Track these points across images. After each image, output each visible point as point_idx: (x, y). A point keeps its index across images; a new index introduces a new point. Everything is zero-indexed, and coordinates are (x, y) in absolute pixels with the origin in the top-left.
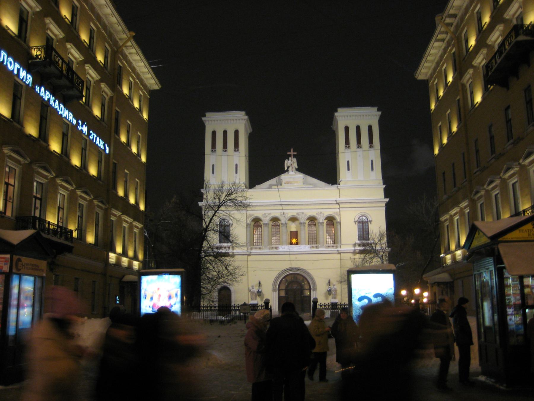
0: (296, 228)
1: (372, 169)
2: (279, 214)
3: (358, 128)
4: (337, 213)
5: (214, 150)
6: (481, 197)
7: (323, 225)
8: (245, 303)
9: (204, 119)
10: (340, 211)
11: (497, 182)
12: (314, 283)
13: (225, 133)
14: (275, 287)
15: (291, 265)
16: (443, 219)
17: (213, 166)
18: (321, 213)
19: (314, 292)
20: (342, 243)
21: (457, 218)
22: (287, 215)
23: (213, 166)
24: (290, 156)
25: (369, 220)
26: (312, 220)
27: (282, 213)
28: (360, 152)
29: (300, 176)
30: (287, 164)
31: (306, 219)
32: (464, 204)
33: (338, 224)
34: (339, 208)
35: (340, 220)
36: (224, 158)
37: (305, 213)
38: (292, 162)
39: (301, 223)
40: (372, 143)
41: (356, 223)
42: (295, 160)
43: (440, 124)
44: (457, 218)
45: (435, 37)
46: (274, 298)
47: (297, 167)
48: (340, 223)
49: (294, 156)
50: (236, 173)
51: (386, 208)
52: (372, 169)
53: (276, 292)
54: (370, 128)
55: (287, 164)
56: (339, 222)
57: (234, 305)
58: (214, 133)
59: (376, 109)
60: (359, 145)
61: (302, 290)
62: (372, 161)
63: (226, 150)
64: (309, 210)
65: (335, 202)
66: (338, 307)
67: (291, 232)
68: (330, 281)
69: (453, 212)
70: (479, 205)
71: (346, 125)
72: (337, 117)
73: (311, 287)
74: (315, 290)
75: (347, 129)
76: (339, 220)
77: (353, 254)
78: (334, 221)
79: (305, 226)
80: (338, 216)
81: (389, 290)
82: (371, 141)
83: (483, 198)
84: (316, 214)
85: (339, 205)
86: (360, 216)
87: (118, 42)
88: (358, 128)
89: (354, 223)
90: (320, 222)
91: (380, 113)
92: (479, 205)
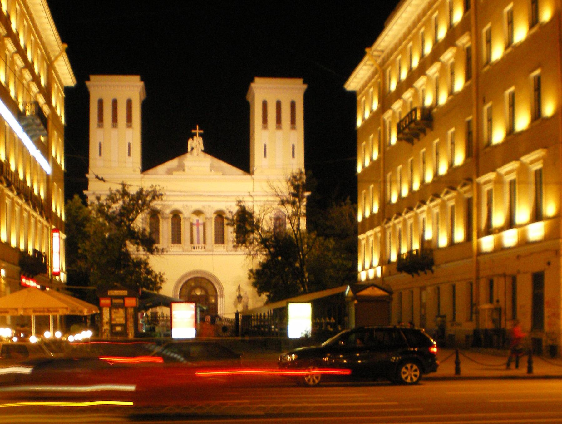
3: (279, 104)
7: (212, 221)
9: (88, 83)
12: (175, 291)
13: (115, 103)
15: (57, 268)
17: (100, 145)
19: (222, 298)
23: (100, 145)
24: (195, 134)
26: (220, 215)
28: (279, 133)
29: (208, 160)
30: (191, 144)
32: (377, 229)
34: (253, 202)
36: (114, 133)
38: (197, 144)
42: (200, 140)
49: (200, 135)
50: (129, 155)
54: (293, 105)
55: (191, 144)
58: (101, 102)
59: (300, 81)
66: (160, 319)
68: (240, 288)
69: (369, 233)
71: (278, 99)
72: (253, 89)
73: (218, 293)
74: (222, 296)
75: (265, 104)
82: (293, 121)
85: (253, 198)
87: (440, 2)
88: (279, 104)
91: (305, 86)
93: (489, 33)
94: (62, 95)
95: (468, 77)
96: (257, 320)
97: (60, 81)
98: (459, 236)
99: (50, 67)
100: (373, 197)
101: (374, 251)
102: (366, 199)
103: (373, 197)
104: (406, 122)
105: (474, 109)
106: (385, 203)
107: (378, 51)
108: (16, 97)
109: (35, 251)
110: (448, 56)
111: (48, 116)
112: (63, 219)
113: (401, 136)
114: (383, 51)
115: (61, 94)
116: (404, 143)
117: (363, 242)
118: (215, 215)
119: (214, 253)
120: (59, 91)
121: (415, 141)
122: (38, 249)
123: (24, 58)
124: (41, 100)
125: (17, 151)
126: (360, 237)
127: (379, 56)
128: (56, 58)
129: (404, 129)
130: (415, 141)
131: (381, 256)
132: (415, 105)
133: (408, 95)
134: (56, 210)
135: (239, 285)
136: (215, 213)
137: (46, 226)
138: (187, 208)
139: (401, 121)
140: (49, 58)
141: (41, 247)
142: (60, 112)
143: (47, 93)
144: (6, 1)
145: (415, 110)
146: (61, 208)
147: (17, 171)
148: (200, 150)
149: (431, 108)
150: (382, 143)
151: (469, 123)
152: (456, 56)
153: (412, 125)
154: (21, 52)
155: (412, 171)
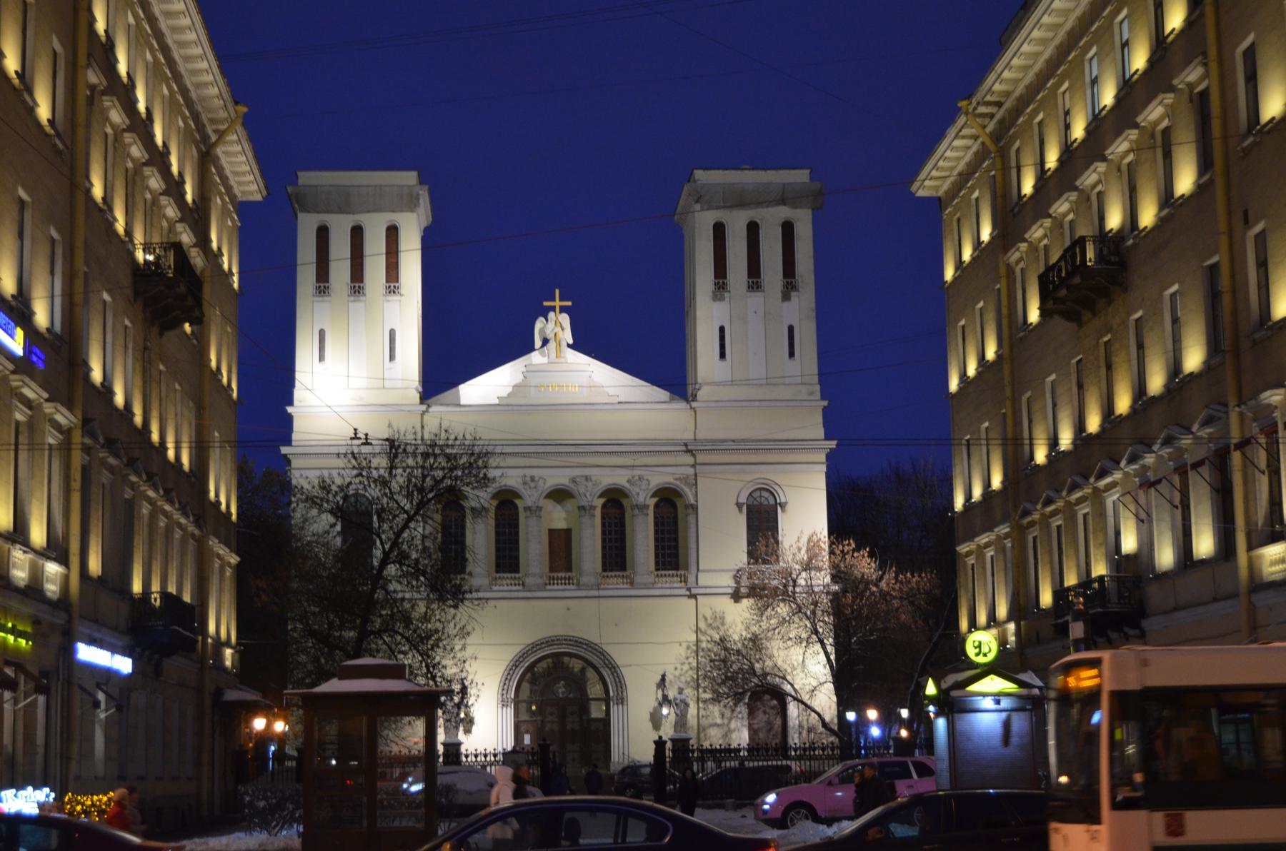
0: (566, 519)
1: (792, 354)
2: (520, 480)
4: (687, 477)
5: (325, 287)
6: (1032, 524)
7: (647, 515)
8: (655, 742)
10: (696, 475)
11: (1058, 504)
14: (505, 692)
16: (963, 549)
18: (640, 478)
19: (620, 706)
20: (701, 568)
21: (990, 553)
22: (541, 483)
25: (778, 501)
26: (615, 501)
27: (528, 479)
28: (756, 299)
31: (598, 494)
32: (1004, 529)
33: (691, 511)
34: (694, 466)
35: (697, 501)
37: (593, 478)
39: (582, 508)
40: (793, 276)
41: (740, 511)
42: (565, 319)
43: (962, 322)
44: (990, 553)
45: (956, 131)
46: (57, 692)
47: (571, 342)
48: (695, 508)
51: (828, 467)
52: (792, 354)
53: (509, 709)
55: (542, 331)
56: (692, 505)
57: (739, 745)
60: (755, 281)
61: (583, 703)
62: (791, 329)
63: (359, 287)
64: (607, 471)
65: (684, 448)
67: (551, 532)
69: (983, 539)
70: (1030, 538)
73: (611, 694)
76: (692, 501)
77: (731, 598)
78: (679, 503)
79: (593, 516)
80: (691, 490)
81: (711, 609)
83: (1037, 527)
84: (629, 481)
85: (694, 455)
86: (752, 489)
89: (736, 509)
90: (637, 505)
92: (1030, 538)
93: (1250, 54)
94: (233, 221)
95: (1205, 165)
96: (414, 454)
97: (229, 189)
98: (1204, 545)
99: (206, 159)
100: (1054, 405)
101: (1040, 568)
102: (972, 457)
103: (1054, 405)
104: (1060, 270)
105: (1224, 240)
106: (1018, 465)
107: (988, 104)
108: (129, 232)
109: (165, 595)
110: (1154, 113)
111: (203, 271)
112: (234, 517)
113: (1050, 304)
114: (999, 104)
115: (233, 220)
116: (1058, 323)
117: (971, 561)
118: (495, 503)
119: (602, 593)
120: (224, 213)
121: (1086, 315)
122: (172, 589)
123: (148, 139)
124: (186, 238)
125: (130, 360)
126: (963, 549)
127: (992, 116)
128: (221, 134)
129: (1056, 288)
130: (1086, 315)
131: (1014, 594)
132: (1082, 231)
133: (1062, 207)
134: (217, 495)
135: (662, 673)
136: (601, 496)
137: (193, 535)
138: (532, 484)
139: (1049, 269)
140: (205, 138)
141: (180, 588)
142: (229, 262)
143: (197, 218)
144: (105, 3)
145: (1081, 242)
146: (231, 491)
147: (128, 405)
148: (564, 344)
149: (1120, 235)
150: (1005, 322)
151: (1214, 269)
152: (1171, 112)
153: (1077, 280)
154: (142, 127)
155: (1080, 387)
